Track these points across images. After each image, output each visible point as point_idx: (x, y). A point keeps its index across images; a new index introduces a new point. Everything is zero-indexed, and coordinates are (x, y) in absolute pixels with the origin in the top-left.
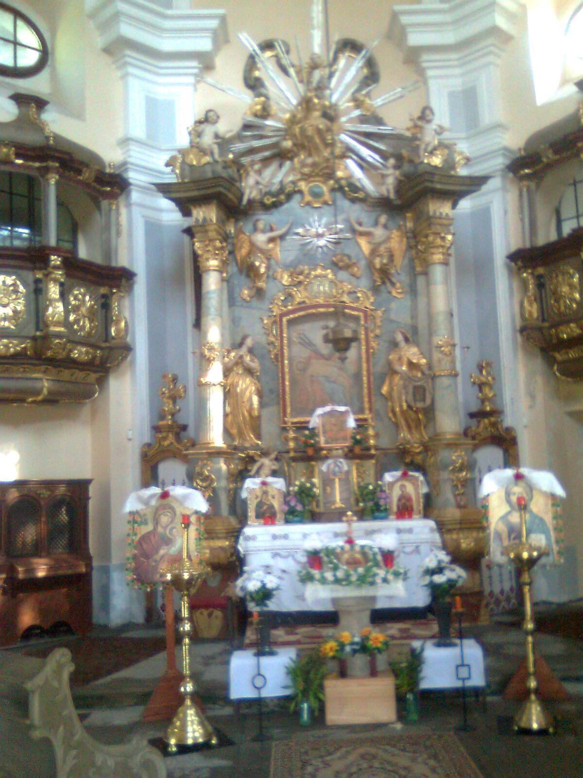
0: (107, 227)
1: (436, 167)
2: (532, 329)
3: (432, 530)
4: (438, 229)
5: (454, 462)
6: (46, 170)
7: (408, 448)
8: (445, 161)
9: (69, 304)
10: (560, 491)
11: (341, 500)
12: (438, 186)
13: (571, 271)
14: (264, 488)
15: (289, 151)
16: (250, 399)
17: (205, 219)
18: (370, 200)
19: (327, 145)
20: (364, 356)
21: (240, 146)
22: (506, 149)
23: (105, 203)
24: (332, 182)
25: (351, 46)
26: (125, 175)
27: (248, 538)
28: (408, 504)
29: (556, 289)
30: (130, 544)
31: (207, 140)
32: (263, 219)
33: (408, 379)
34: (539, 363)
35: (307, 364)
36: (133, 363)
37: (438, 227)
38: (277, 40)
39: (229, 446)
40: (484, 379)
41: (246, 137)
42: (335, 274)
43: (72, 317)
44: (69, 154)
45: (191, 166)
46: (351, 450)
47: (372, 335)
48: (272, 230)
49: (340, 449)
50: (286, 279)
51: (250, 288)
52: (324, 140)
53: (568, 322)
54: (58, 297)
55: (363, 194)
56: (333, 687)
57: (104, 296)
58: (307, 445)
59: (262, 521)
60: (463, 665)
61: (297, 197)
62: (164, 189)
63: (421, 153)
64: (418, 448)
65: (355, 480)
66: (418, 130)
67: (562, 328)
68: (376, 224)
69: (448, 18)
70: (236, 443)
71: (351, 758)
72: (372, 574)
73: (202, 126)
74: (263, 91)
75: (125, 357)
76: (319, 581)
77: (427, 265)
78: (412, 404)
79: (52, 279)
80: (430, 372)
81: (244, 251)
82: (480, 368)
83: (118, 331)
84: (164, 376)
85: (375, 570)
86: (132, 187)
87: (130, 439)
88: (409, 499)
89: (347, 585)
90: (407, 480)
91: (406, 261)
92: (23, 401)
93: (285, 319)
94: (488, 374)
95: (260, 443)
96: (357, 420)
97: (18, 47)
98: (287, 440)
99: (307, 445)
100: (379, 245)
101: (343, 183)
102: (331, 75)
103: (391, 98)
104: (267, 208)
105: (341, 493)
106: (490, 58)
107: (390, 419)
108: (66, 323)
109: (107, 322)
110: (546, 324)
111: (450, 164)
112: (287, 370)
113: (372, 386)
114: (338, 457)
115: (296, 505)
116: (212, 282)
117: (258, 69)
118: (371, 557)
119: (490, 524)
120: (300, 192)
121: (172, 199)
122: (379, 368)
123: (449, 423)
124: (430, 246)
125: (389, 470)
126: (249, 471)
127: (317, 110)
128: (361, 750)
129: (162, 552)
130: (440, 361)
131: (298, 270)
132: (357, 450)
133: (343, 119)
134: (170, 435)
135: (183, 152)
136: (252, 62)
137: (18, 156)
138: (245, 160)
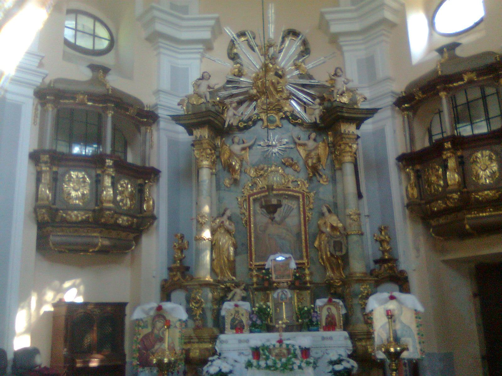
0: (144, 142)
1: (345, 104)
3: (346, 338)
5: (361, 292)
6: (105, 109)
7: (332, 283)
8: (351, 100)
9: (117, 189)
10: (420, 308)
11: (286, 317)
12: (346, 115)
13: (437, 167)
14: (237, 309)
16: (228, 250)
17: (201, 136)
18: (305, 124)
19: (278, 92)
21: (224, 93)
22: (393, 92)
23: (143, 129)
24: (281, 114)
25: (294, 33)
26: (156, 112)
27: (222, 342)
30: (136, 341)
31: (203, 89)
32: (239, 136)
33: (330, 236)
34: (420, 227)
35: (266, 227)
36: (157, 227)
38: (247, 31)
39: (214, 280)
40: (382, 238)
41: (229, 87)
42: (284, 170)
43: (118, 198)
44: (120, 99)
45: (193, 105)
46: (293, 283)
47: (307, 208)
48: (244, 143)
49: (285, 282)
50: (252, 173)
51: (230, 179)
52: (275, 89)
53: (437, 200)
54: (110, 185)
55: (301, 121)
57: (140, 185)
59: (234, 331)
61: (260, 123)
62: (176, 119)
64: (338, 283)
66: (333, 81)
67: (433, 204)
69: (355, 15)
70: (219, 279)
73: (201, 81)
74: (239, 60)
75: (152, 223)
76: (255, 367)
77: (341, 163)
78: (334, 253)
79: (106, 174)
81: (226, 156)
82: (381, 230)
83: (148, 207)
84: (176, 235)
85: (293, 360)
86: (160, 119)
87: (154, 277)
90: (332, 305)
91: (329, 162)
92: (86, 251)
93: (251, 199)
94: (386, 234)
95: (234, 278)
96: (297, 264)
97: (96, 39)
98: (252, 276)
99: (263, 280)
100: (311, 151)
101: (288, 114)
102: (280, 51)
103: (317, 64)
104: (241, 130)
105: (286, 312)
107: (320, 263)
108: (114, 201)
109: (142, 200)
110: (423, 202)
111: (353, 101)
112: (252, 231)
114: (284, 288)
115: (257, 321)
116: (205, 174)
117: (236, 48)
119: (375, 330)
120: (262, 120)
121: (181, 125)
122: (312, 229)
124: (342, 152)
125: (319, 297)
126: (227, 297)
127: (272, 71)
129: (157, 347)
132: (297, 284)
133: (288, 77)
134: (179, 273)
135: (189, 97)
136: (232, 44)
137: (89, 100)
138: (227, 101)
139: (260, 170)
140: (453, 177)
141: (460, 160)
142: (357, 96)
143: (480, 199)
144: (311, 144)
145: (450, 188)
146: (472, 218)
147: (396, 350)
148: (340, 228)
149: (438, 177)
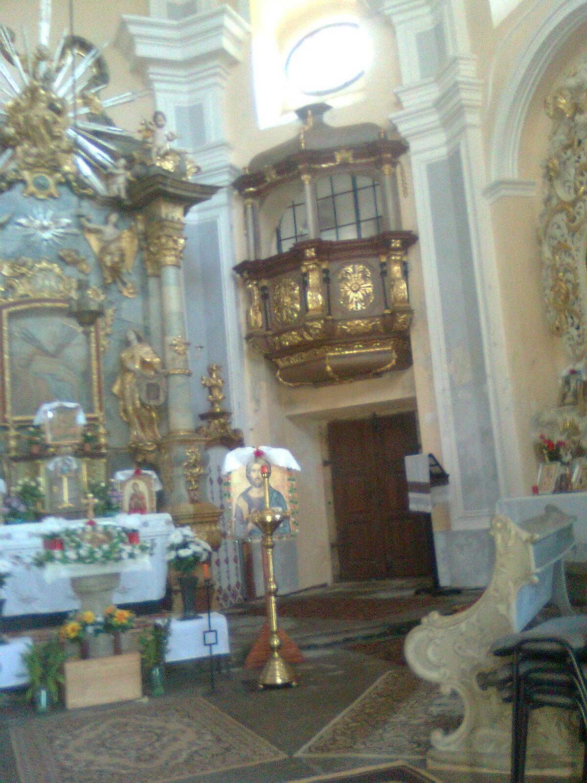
1: (167, 171)
2: (258, 336)
3: (167, 523)
4: (171, 232)
5: (188, 458)
7: (142, 447)
8: (177, 167)
10: (295, 466)
11: (69, 499)
12: (171, 190)
15: (11, 138)
19: (55, 138)
20: (94, 353)
22: (231, 167)
24: (59, 175)
28: (140, 502)
29: (279, 300)
34: (262, 369)
35: (30, 360)
37: (171, 230)
40: (214, 382)
47: (102, 333)
52: (50, 132)
56: (75, 669)
58: (31, 442)
60: (210, 631)
61: (20, 186)
63: (154, 156)
64: (150, 446)
65: (85, 479)
68: (106, 222)
69: (176, 34)
71: (102, 728)
72: (117, 550)
77: (159, 266)
78: (145, 401)
80: (164, 370)
82: (210, 371)
85: (121, 545)
88: (142, 498)
89: (90, 563)
91: (137, 263)
94: (218, 377)
96: (88, 419)
99: (31, 442)
100: (109, 242)
101: (71, 177)
102: (58, 70)
105: (70, 491)
106: (218, 79)
107: (121, 418)
111: (181, 170)
113: (103, 385)
114: (67, 454)
118: (116, 535)
119: (232, 500)
120: (23, 182)
122: (110, 366)
123: (182, 421)
124: (163, 247)
127: (43, 102)
128: (112, 721)
130: (173, 359)
131: (21, 261)
139: (19, 265)
140: (315, 299)
141: (324, 275)
142: (187, 163)
143: (349, 330)
144: (109, 231)
145: (310, 314)
146: (335, 356)
147: (273, 518)
148: (156, 364)
149: (293, 297)
